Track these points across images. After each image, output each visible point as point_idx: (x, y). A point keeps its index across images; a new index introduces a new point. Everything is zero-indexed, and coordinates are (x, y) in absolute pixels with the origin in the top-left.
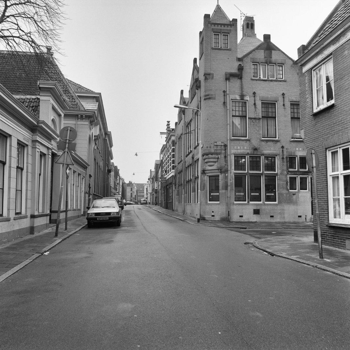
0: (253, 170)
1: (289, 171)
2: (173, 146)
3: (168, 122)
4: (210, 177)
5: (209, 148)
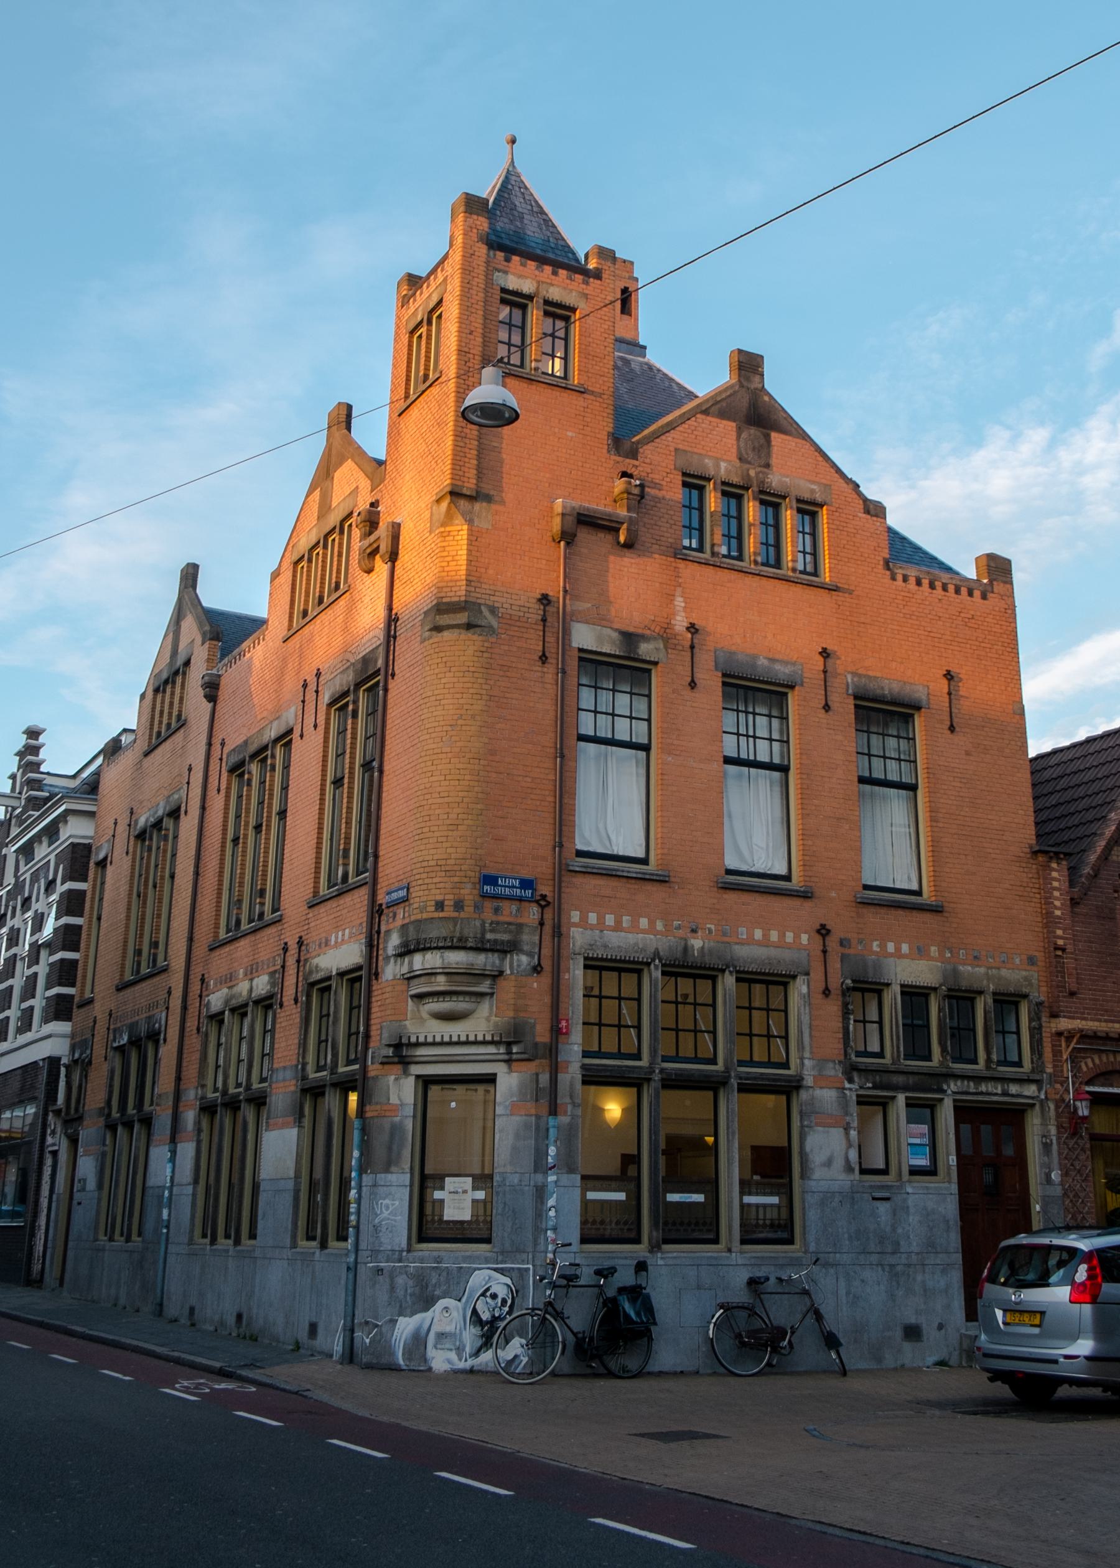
2: (69, 877)
4: (426, 1082)
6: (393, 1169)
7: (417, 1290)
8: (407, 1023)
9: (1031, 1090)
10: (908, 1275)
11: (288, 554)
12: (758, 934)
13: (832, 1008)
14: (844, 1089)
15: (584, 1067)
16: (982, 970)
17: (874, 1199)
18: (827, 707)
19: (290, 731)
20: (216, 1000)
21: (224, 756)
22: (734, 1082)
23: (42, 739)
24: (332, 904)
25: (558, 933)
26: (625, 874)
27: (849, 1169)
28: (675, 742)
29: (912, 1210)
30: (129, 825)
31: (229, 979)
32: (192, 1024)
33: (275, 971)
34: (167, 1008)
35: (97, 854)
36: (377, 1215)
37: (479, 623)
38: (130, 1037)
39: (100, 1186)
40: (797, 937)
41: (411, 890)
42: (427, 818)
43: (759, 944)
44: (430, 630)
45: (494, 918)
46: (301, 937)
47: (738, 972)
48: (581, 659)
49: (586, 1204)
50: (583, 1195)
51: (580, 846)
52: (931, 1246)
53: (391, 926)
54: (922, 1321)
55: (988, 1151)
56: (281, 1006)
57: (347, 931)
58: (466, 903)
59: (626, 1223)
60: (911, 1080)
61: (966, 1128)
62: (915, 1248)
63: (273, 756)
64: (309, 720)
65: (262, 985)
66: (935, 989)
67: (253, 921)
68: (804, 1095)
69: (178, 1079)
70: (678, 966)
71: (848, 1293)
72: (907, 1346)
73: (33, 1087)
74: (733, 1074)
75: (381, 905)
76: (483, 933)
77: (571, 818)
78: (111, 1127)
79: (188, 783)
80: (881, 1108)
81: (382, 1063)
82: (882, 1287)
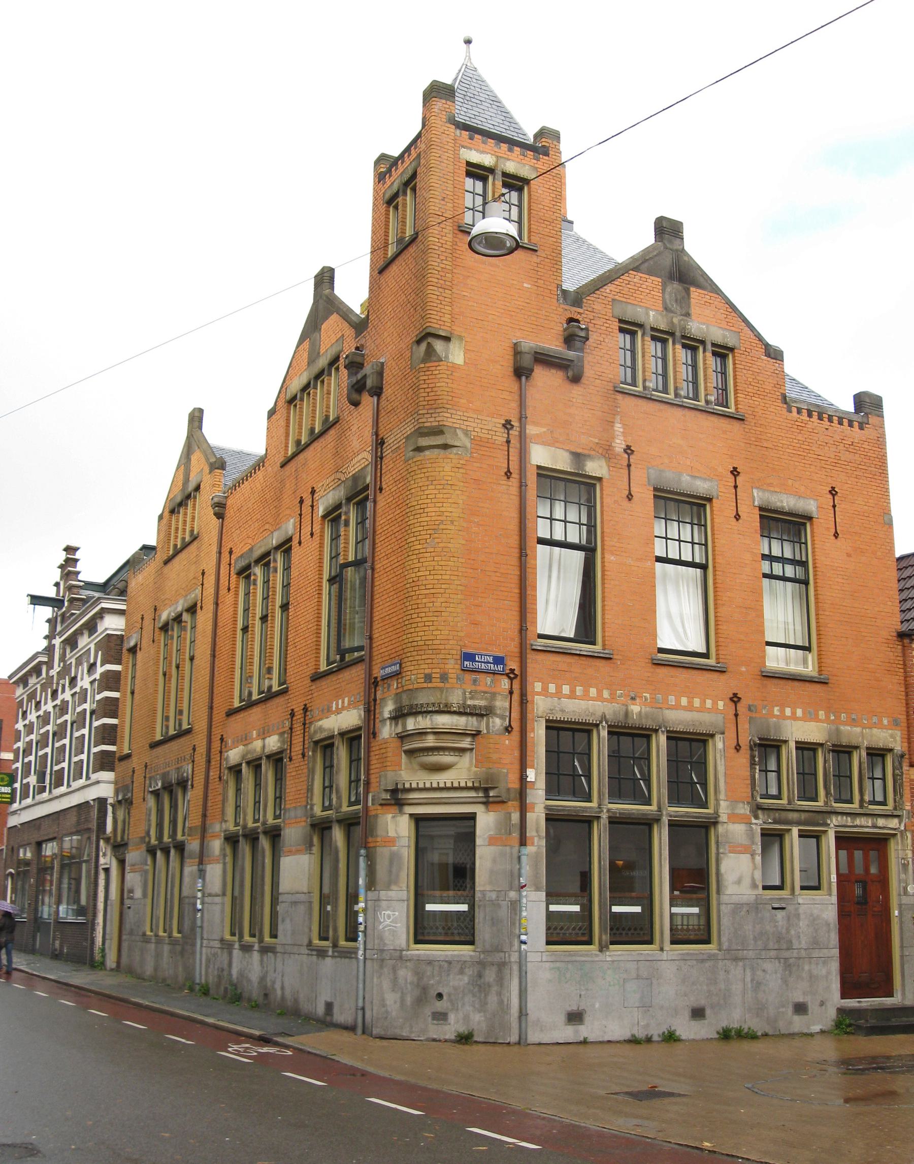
0: (620, 797)
1: (759, 807)
3: (70, 550)
4: (418, 820)
5: (436, 683)
6: (393, 887)
7: (415, 980)
8: (402, 772)
9: (894, 823)
10: (798, 966)
11: (283, 395)
12: (684, 701)
13: (743, 759)
14: (751, 824)
15: (547, 808)
16: (858, 730)
17: (773, 908)
18: (737, 517)
19: (290, 540)
20: (234, 755)
21: (233, 562)
22: (665, 820)
23: (78, 555)
24: (333, 678)
25: (524, 702)
26: (578, 652)
27: (754, 886)
28: (617, 544)
29: (802, 917)
30: (154, 620)
31: (245, 739)
32: (214, 774)
33: (284, 732)
34: (193, 761)
35: (129, 643)
36: (381, 923)
37: (456, 444)
38: (163, 784)
39: (145, 895)
40: (715, 703)
41: (404, 665)
42: (416, 606)
43: (685, 708)
44: (414, 450)
45: (473, 688)
46: (305, 705)
47: (668, 732)
48: (539, 475)
49: (550, 916)
50: (547, 908)
51: (540, 631)
52: (815, 944)
53: (386, 695)
54: (808, 999)
55: (859, 869)
56: (291, 759)
57: (346, 700)
58: (451, 676)
59: (580, 929)
60: (803, 816)
61: (843, 853)
62: (804, 945)
63: (275, 561)
64: (306, 530)
65: (273, 743)
66: (821, 745)
67: (263, 692)
68: (721, 829)
69: (204, 816)
70: (621, 727)
71: (752, 980)
72: (796, 1018)
73: (87, 820)
74: (664, 813)
75: (376, 678)
76: (465, 699)
77: (533, 606)
78: (152, 852)
79: (202, 585)
80: (778, 838)
81: (381, 805)
82: (779, 975)
